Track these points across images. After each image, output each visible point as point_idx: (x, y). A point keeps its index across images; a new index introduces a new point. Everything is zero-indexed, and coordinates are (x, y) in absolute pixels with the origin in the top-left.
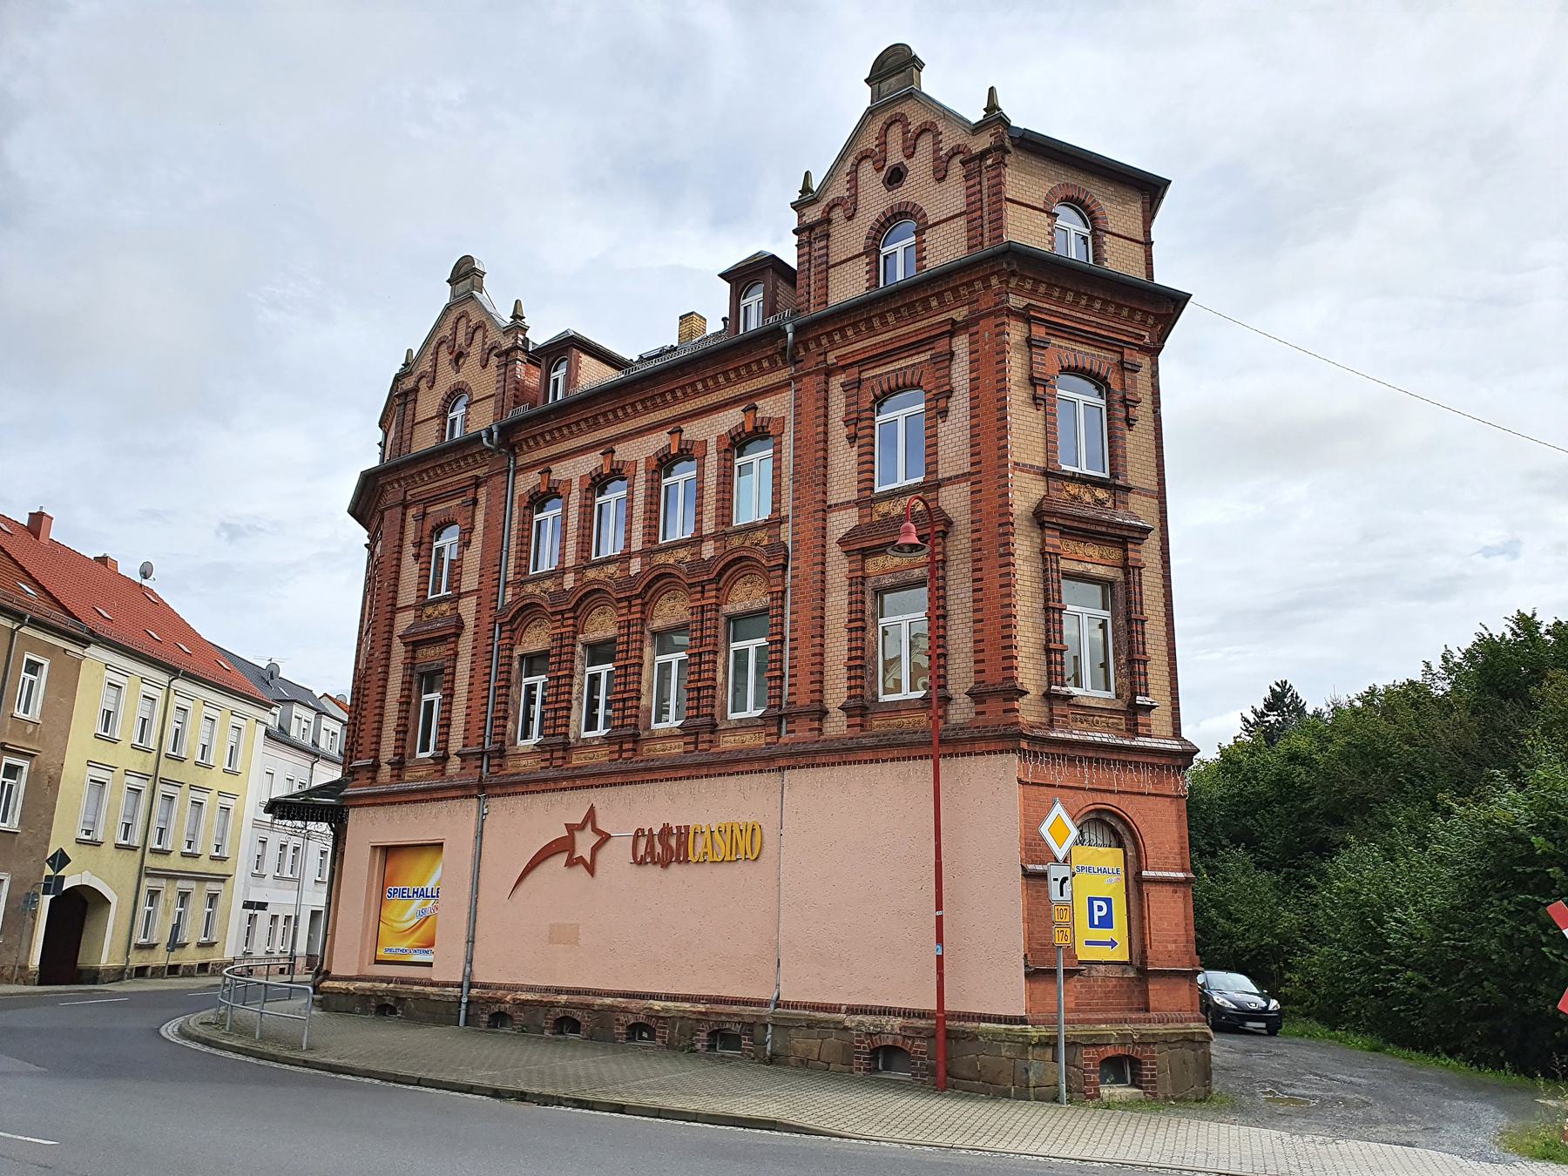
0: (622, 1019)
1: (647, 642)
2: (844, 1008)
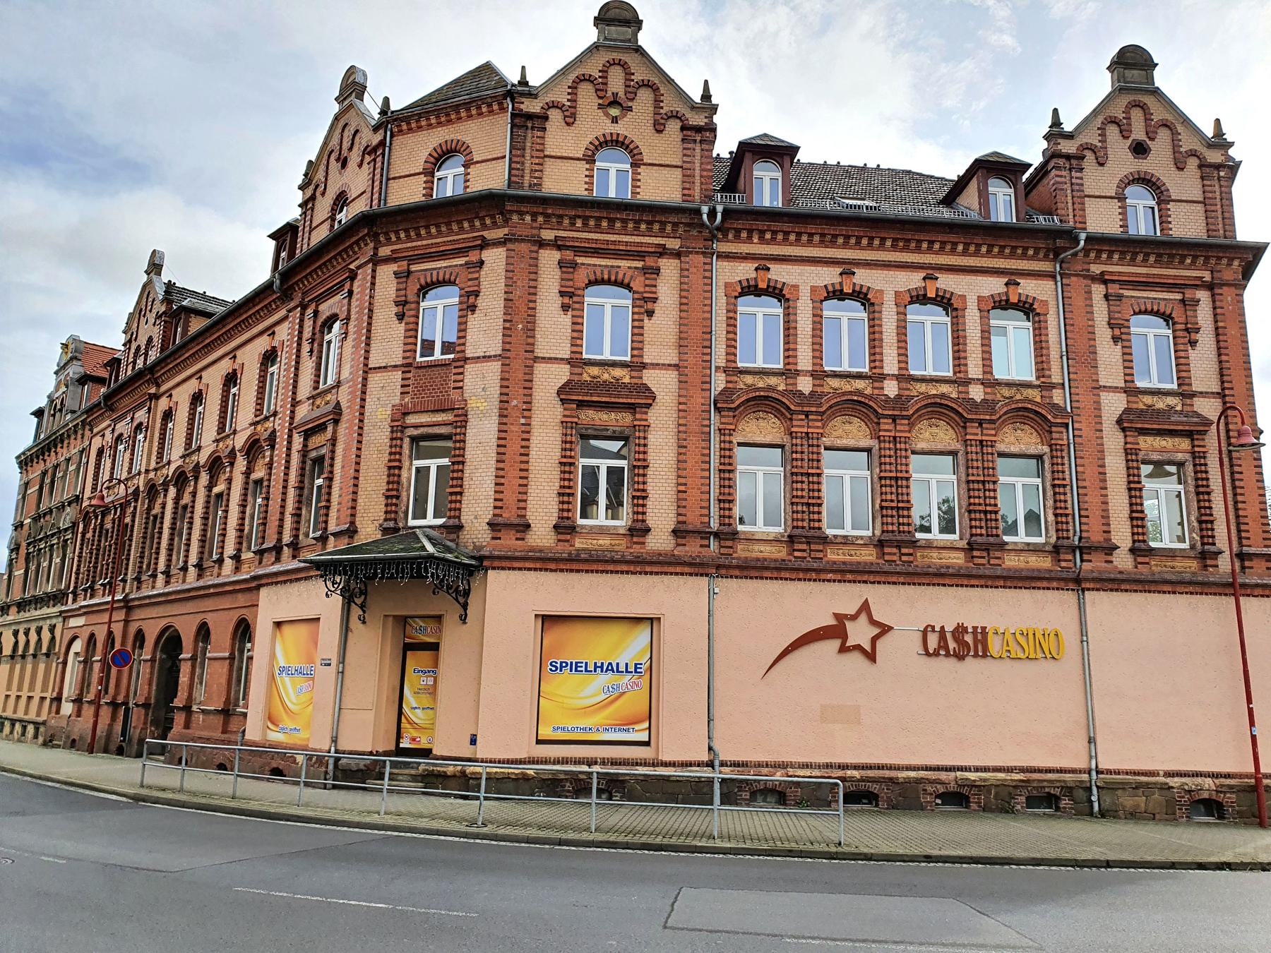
0: (929, 789)
2: (1161, 773)
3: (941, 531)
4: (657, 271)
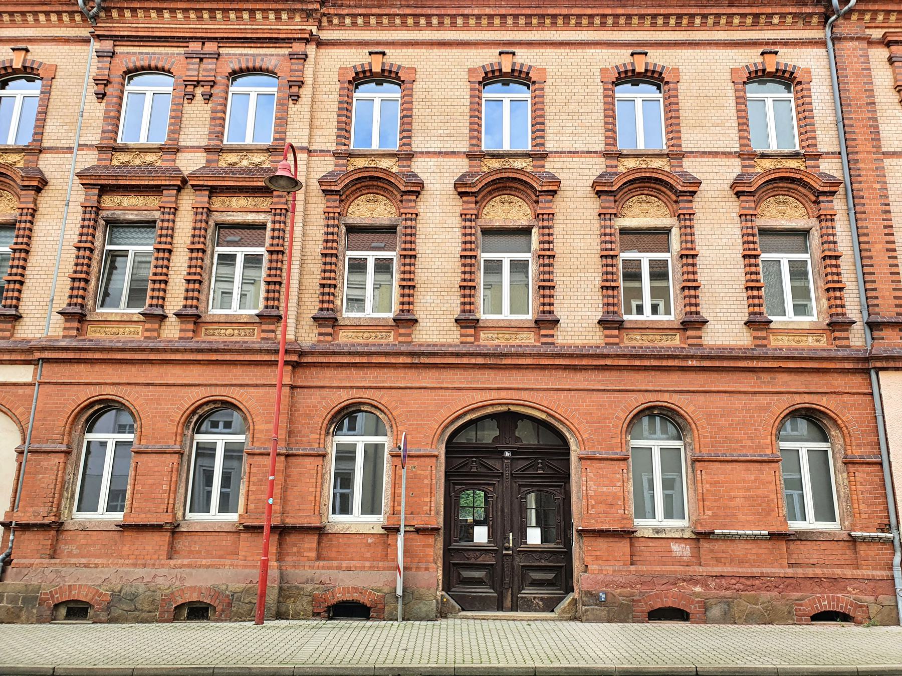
1: (100, 229)
4: (305, 57)
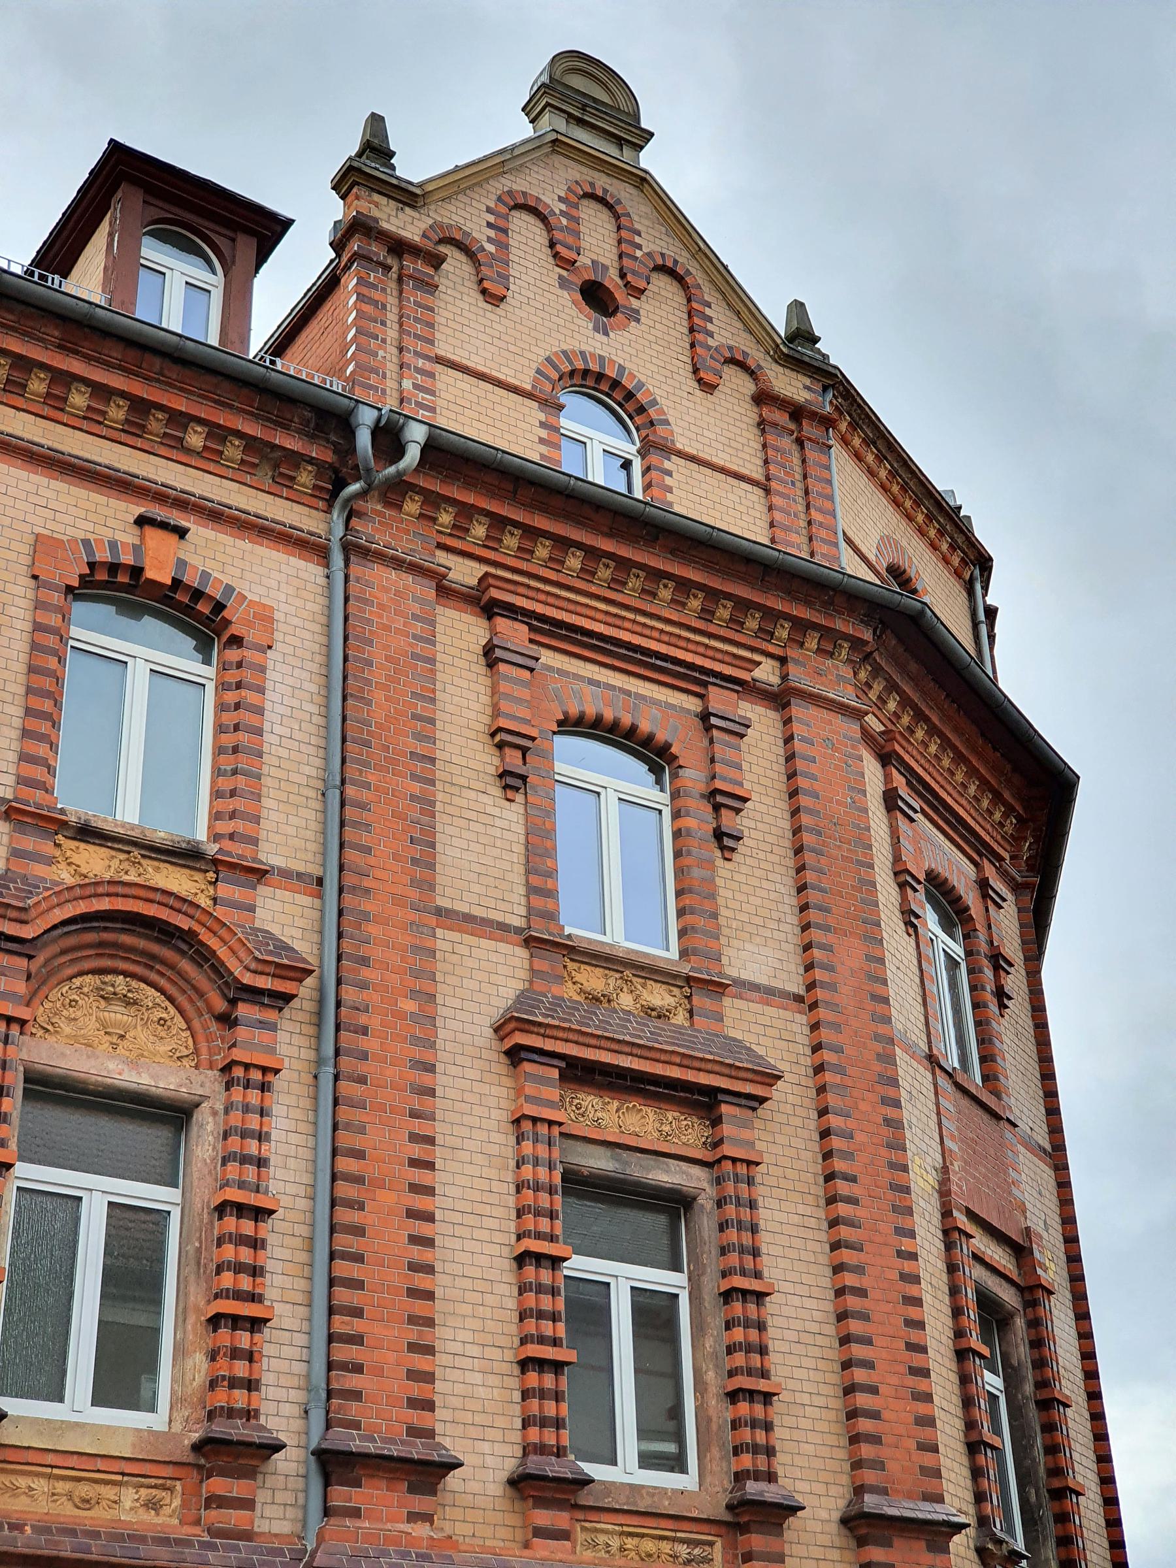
3: (100, 1398)
